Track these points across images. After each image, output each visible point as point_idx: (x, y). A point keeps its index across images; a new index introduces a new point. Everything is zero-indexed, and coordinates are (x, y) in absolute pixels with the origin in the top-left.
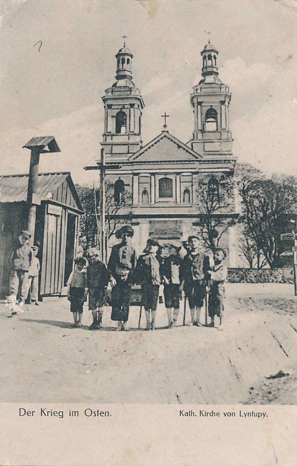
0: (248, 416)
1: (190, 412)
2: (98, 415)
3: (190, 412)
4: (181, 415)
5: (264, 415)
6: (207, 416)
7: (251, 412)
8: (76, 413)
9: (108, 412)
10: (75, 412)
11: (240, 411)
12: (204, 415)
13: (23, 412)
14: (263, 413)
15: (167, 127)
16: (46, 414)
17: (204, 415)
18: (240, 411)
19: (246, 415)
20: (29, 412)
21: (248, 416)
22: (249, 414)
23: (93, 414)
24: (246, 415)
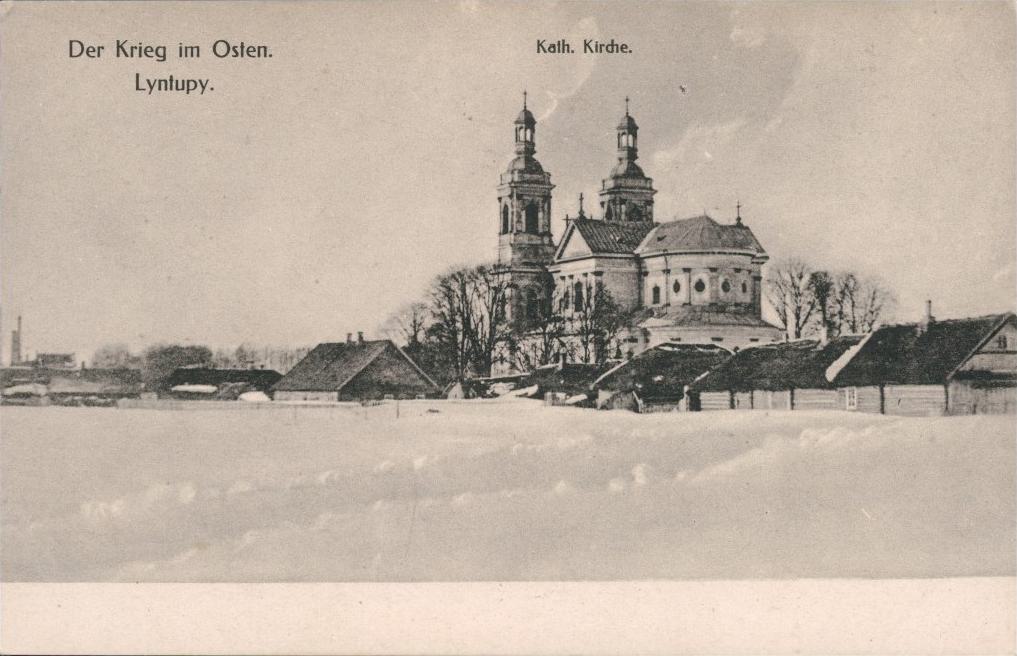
0: (160, 89)
1: (559, 44)
2: (242, 55)
3: (559, 44)
4: (588, 49)
5: (204, 88)
6: (601, 51)
7: (168, 79)
8: (195, 50)
9: (265, 48)
10: (192, 48)
11: (138, 75)
12: (594, 49)
13: (77, 49)
14: (200, 81)
15: (658, 285)
16: (129, 53)
17: (594, 49)
18: (138, 75)
19: (152, 88)
20: (91, 49)
21: (160, 89)
22: (163, 83)
23: (232, 53)
24: (152, 88)
